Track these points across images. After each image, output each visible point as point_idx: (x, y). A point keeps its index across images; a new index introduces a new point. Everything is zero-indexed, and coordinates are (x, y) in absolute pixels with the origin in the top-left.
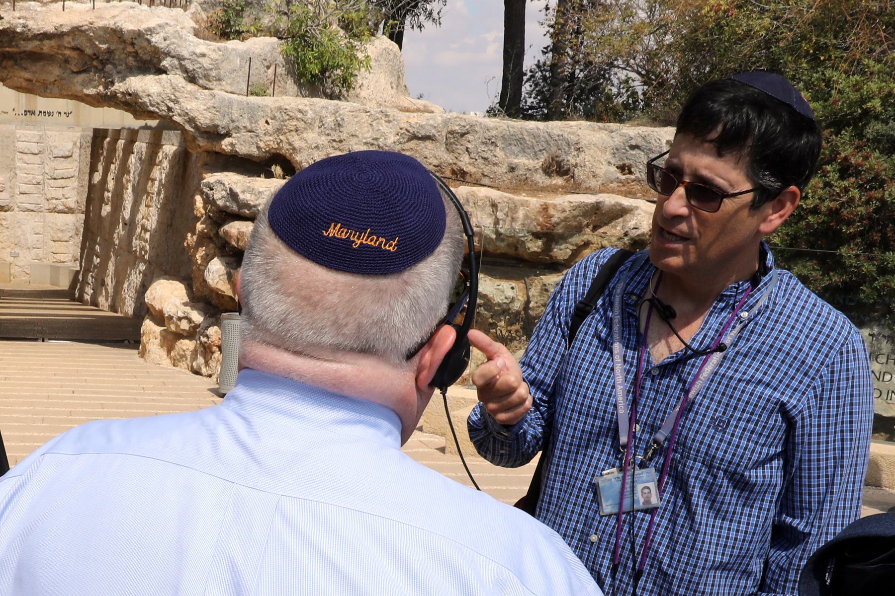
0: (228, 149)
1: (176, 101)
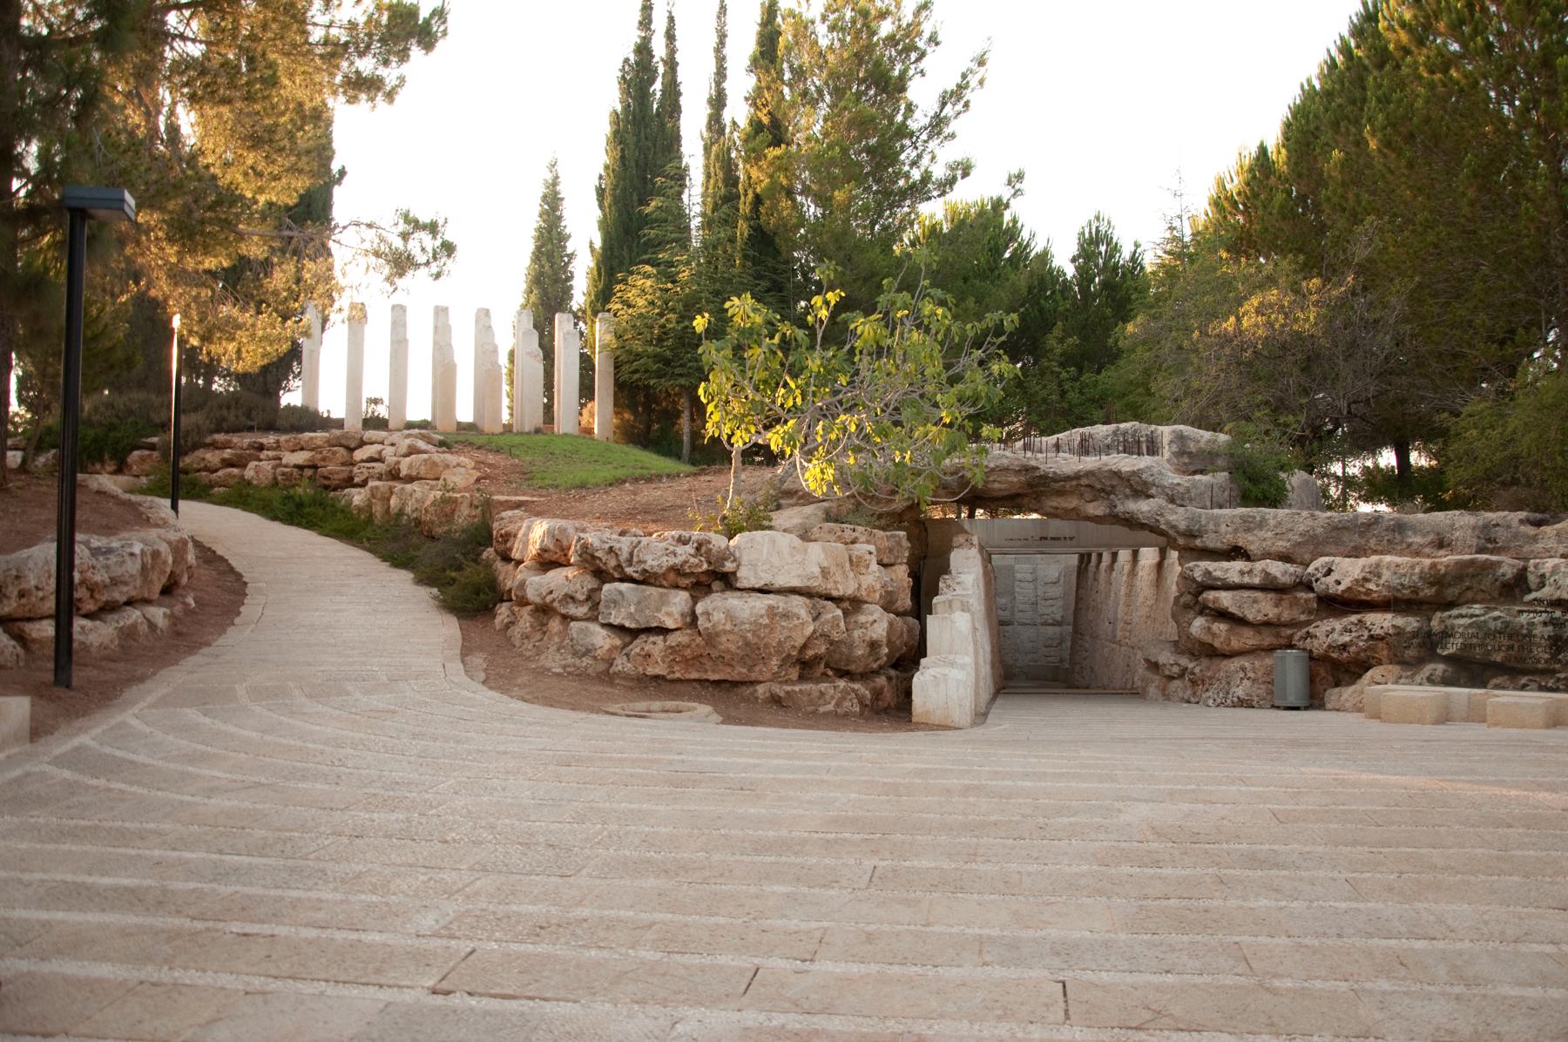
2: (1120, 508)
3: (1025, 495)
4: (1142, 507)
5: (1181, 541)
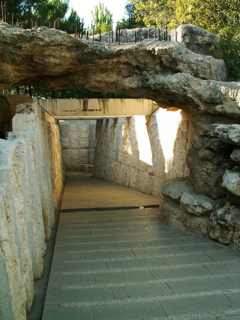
0: (220, 110)
2: (151, 81)
3: (76, 73)
4: (172, 80)
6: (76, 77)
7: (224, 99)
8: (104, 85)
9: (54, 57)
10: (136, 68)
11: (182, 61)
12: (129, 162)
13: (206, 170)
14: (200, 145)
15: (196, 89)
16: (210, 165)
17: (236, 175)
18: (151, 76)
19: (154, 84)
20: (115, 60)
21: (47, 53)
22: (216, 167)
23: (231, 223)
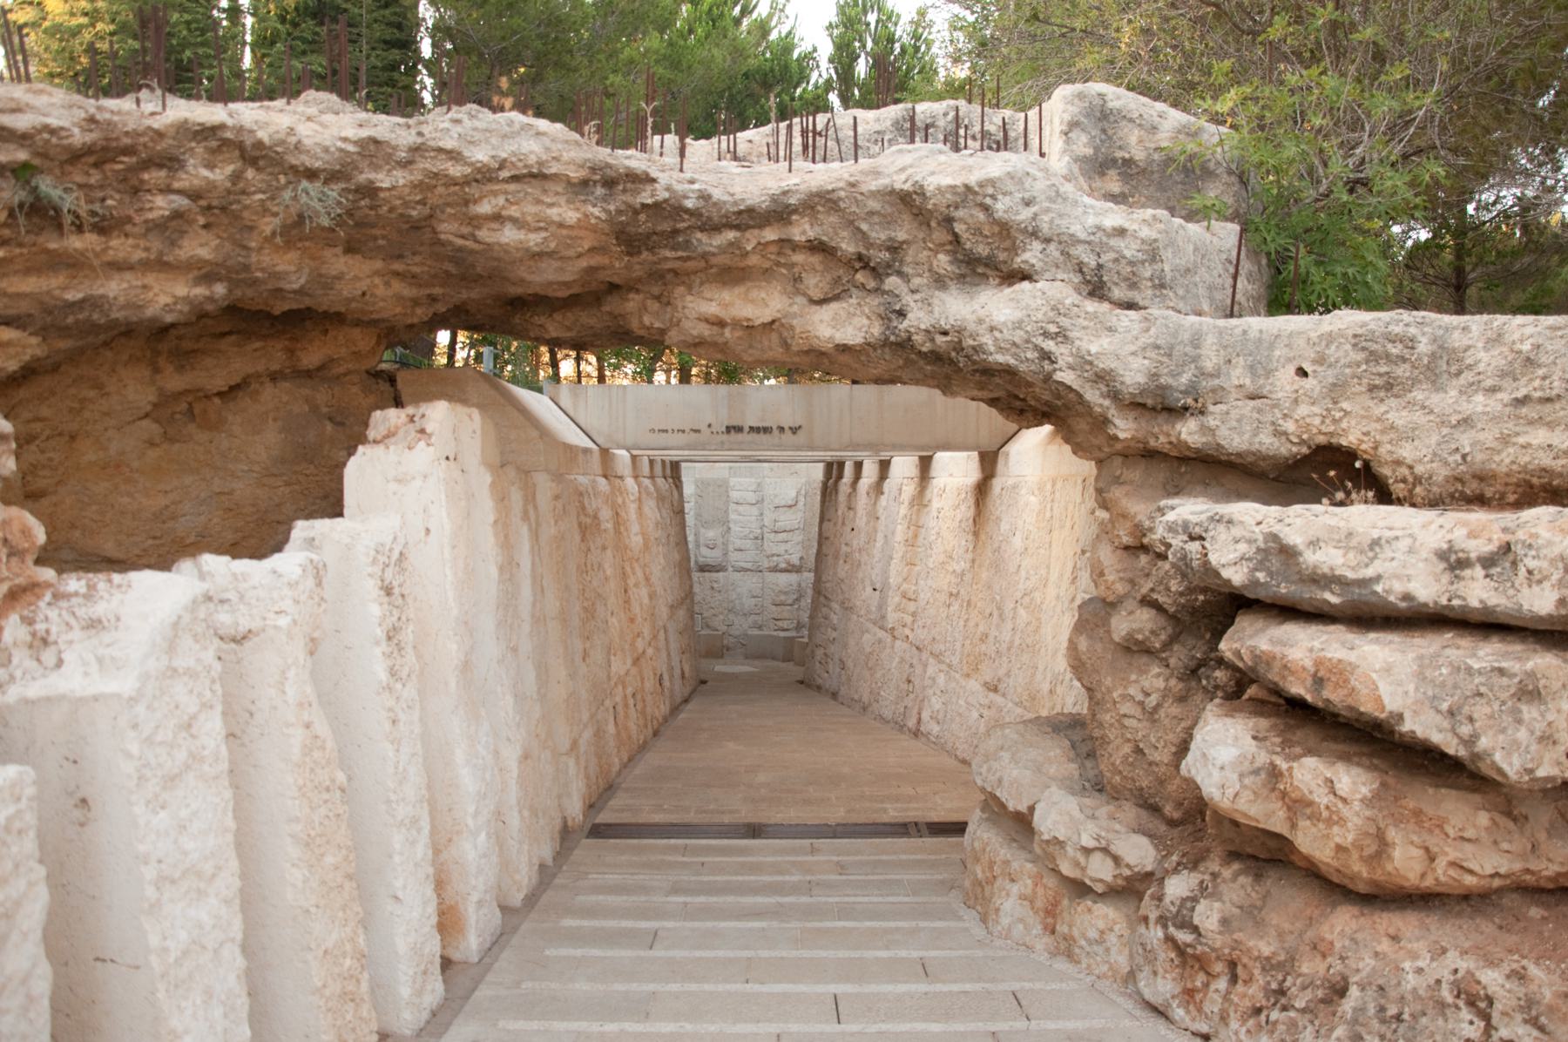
1: (1062, 336)
2: (918, 319)
4: (994, 315)
5: (1124, 427)
6: (632, 302)
7: (1213, 391)
8: (739, 333)
9: (518, 223)
10: (857, 265)
11: (1035, 234)
12: (921, 635)
13: (1140, 697)
14: (1120, 588)
15: (1094, 350)
16: (1159, 675)
17: (1239, 727)
18: (917, 296)
19: (927, 331)
20: (770, 234)
21: (485, 208)
22: (1181, 685)
23: (1218, 944)
